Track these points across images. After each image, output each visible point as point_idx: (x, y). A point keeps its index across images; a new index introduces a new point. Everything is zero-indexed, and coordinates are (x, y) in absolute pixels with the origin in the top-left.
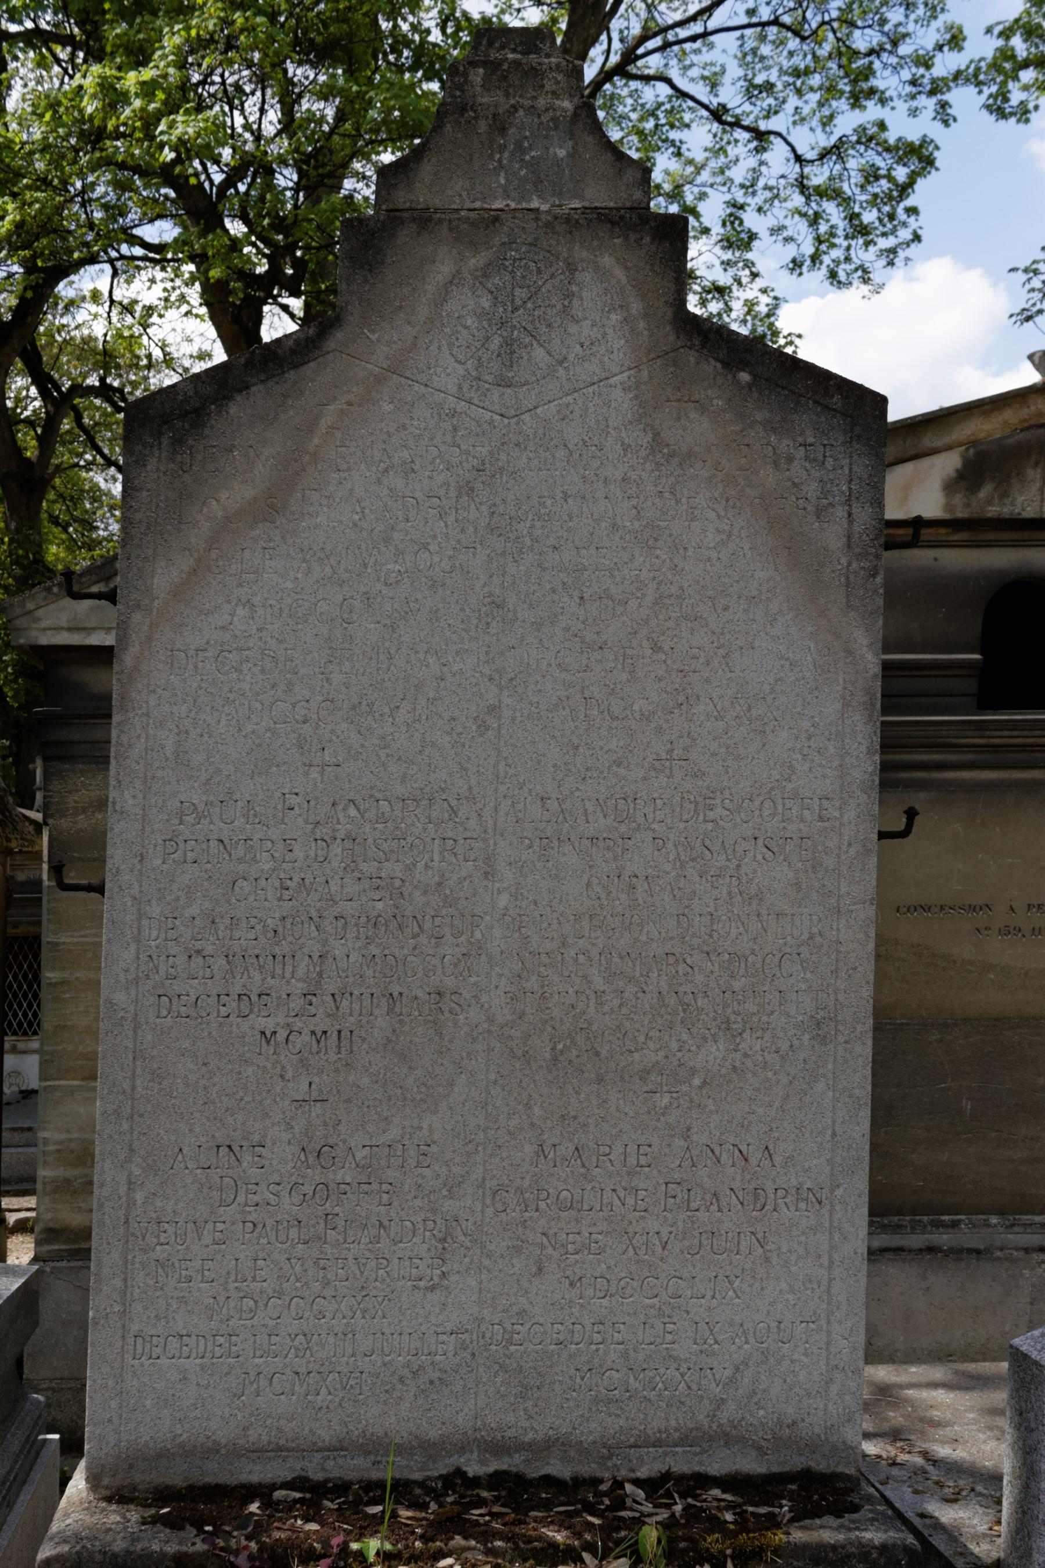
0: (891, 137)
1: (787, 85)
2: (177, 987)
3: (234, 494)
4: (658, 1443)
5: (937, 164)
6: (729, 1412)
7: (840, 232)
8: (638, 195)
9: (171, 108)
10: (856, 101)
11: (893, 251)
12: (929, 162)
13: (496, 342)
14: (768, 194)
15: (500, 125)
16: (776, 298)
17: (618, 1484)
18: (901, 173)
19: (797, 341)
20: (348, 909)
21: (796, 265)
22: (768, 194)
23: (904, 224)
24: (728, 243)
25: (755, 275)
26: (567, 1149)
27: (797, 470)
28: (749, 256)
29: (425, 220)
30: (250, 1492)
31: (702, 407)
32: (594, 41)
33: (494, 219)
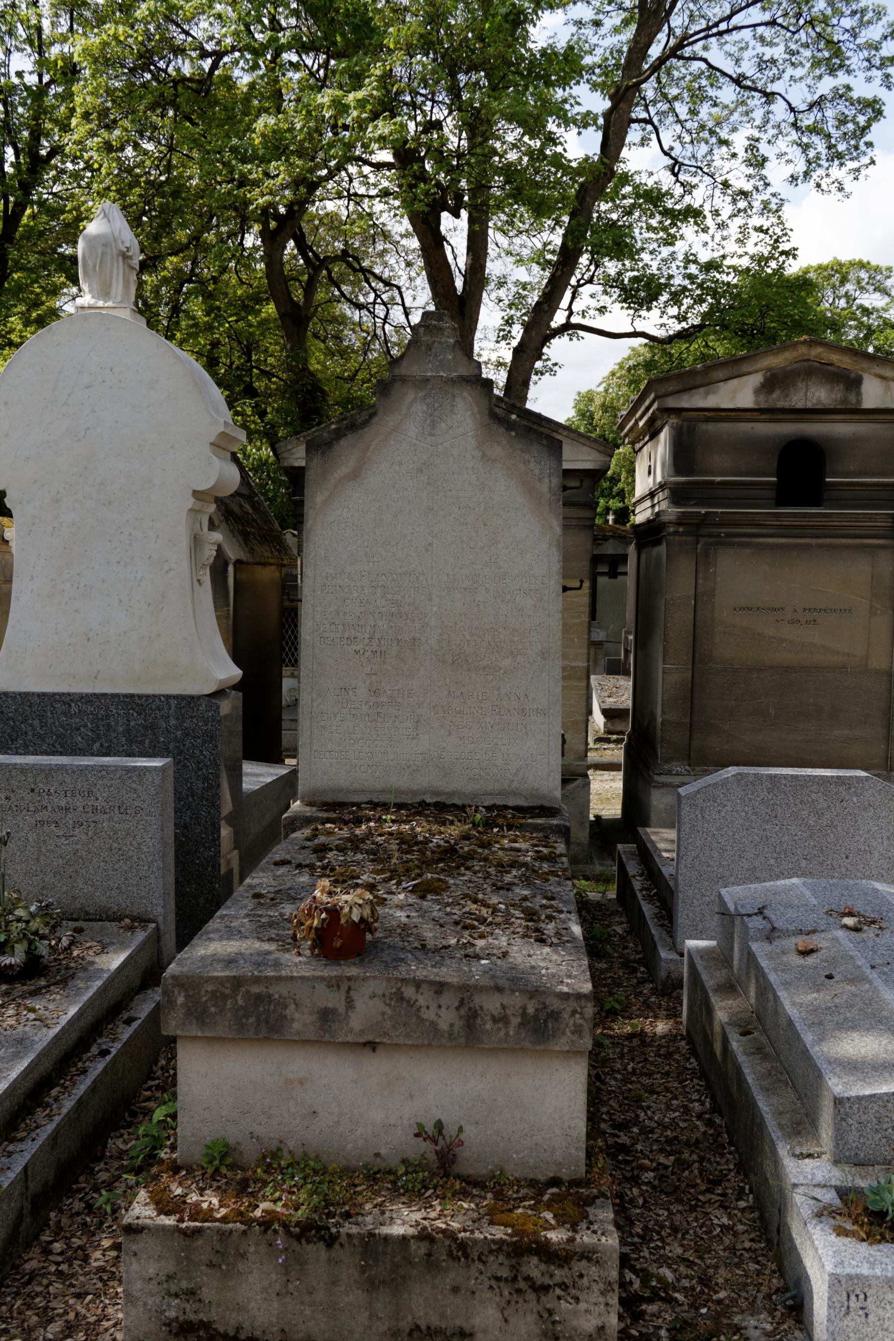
0: (855, 95)
1: (785, 61)
2: (326, 635)
3: (342, 471)
4: (491, 794)
5: (885, 114)
6: (515, 785)
7: (823, 157)
8: (476, 371)
9: (375, 116)
10: (832, 71)
11: (858, 170)
12: (878, 114)
13: (429, 421)
14: (775, 131)
15: (429, 348)
16: (782, 200)
17: (477, 807)
18: (862, 120)
19: (789, 233)
20: (383, 610)
21: (793, 179)
22: (775, 131)
23: (864, 153)
24: (749, 163)
25: (767, 185)
26: (458, 693)
27: (532, 465)
28: (763, 172)
29: (404, 380)
30: (353, 804)
31: (499, 443)
32: (659, 30)
33: (426, 380)
